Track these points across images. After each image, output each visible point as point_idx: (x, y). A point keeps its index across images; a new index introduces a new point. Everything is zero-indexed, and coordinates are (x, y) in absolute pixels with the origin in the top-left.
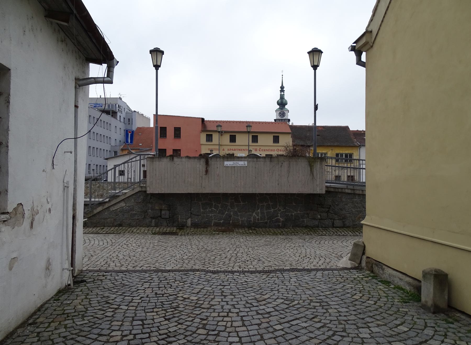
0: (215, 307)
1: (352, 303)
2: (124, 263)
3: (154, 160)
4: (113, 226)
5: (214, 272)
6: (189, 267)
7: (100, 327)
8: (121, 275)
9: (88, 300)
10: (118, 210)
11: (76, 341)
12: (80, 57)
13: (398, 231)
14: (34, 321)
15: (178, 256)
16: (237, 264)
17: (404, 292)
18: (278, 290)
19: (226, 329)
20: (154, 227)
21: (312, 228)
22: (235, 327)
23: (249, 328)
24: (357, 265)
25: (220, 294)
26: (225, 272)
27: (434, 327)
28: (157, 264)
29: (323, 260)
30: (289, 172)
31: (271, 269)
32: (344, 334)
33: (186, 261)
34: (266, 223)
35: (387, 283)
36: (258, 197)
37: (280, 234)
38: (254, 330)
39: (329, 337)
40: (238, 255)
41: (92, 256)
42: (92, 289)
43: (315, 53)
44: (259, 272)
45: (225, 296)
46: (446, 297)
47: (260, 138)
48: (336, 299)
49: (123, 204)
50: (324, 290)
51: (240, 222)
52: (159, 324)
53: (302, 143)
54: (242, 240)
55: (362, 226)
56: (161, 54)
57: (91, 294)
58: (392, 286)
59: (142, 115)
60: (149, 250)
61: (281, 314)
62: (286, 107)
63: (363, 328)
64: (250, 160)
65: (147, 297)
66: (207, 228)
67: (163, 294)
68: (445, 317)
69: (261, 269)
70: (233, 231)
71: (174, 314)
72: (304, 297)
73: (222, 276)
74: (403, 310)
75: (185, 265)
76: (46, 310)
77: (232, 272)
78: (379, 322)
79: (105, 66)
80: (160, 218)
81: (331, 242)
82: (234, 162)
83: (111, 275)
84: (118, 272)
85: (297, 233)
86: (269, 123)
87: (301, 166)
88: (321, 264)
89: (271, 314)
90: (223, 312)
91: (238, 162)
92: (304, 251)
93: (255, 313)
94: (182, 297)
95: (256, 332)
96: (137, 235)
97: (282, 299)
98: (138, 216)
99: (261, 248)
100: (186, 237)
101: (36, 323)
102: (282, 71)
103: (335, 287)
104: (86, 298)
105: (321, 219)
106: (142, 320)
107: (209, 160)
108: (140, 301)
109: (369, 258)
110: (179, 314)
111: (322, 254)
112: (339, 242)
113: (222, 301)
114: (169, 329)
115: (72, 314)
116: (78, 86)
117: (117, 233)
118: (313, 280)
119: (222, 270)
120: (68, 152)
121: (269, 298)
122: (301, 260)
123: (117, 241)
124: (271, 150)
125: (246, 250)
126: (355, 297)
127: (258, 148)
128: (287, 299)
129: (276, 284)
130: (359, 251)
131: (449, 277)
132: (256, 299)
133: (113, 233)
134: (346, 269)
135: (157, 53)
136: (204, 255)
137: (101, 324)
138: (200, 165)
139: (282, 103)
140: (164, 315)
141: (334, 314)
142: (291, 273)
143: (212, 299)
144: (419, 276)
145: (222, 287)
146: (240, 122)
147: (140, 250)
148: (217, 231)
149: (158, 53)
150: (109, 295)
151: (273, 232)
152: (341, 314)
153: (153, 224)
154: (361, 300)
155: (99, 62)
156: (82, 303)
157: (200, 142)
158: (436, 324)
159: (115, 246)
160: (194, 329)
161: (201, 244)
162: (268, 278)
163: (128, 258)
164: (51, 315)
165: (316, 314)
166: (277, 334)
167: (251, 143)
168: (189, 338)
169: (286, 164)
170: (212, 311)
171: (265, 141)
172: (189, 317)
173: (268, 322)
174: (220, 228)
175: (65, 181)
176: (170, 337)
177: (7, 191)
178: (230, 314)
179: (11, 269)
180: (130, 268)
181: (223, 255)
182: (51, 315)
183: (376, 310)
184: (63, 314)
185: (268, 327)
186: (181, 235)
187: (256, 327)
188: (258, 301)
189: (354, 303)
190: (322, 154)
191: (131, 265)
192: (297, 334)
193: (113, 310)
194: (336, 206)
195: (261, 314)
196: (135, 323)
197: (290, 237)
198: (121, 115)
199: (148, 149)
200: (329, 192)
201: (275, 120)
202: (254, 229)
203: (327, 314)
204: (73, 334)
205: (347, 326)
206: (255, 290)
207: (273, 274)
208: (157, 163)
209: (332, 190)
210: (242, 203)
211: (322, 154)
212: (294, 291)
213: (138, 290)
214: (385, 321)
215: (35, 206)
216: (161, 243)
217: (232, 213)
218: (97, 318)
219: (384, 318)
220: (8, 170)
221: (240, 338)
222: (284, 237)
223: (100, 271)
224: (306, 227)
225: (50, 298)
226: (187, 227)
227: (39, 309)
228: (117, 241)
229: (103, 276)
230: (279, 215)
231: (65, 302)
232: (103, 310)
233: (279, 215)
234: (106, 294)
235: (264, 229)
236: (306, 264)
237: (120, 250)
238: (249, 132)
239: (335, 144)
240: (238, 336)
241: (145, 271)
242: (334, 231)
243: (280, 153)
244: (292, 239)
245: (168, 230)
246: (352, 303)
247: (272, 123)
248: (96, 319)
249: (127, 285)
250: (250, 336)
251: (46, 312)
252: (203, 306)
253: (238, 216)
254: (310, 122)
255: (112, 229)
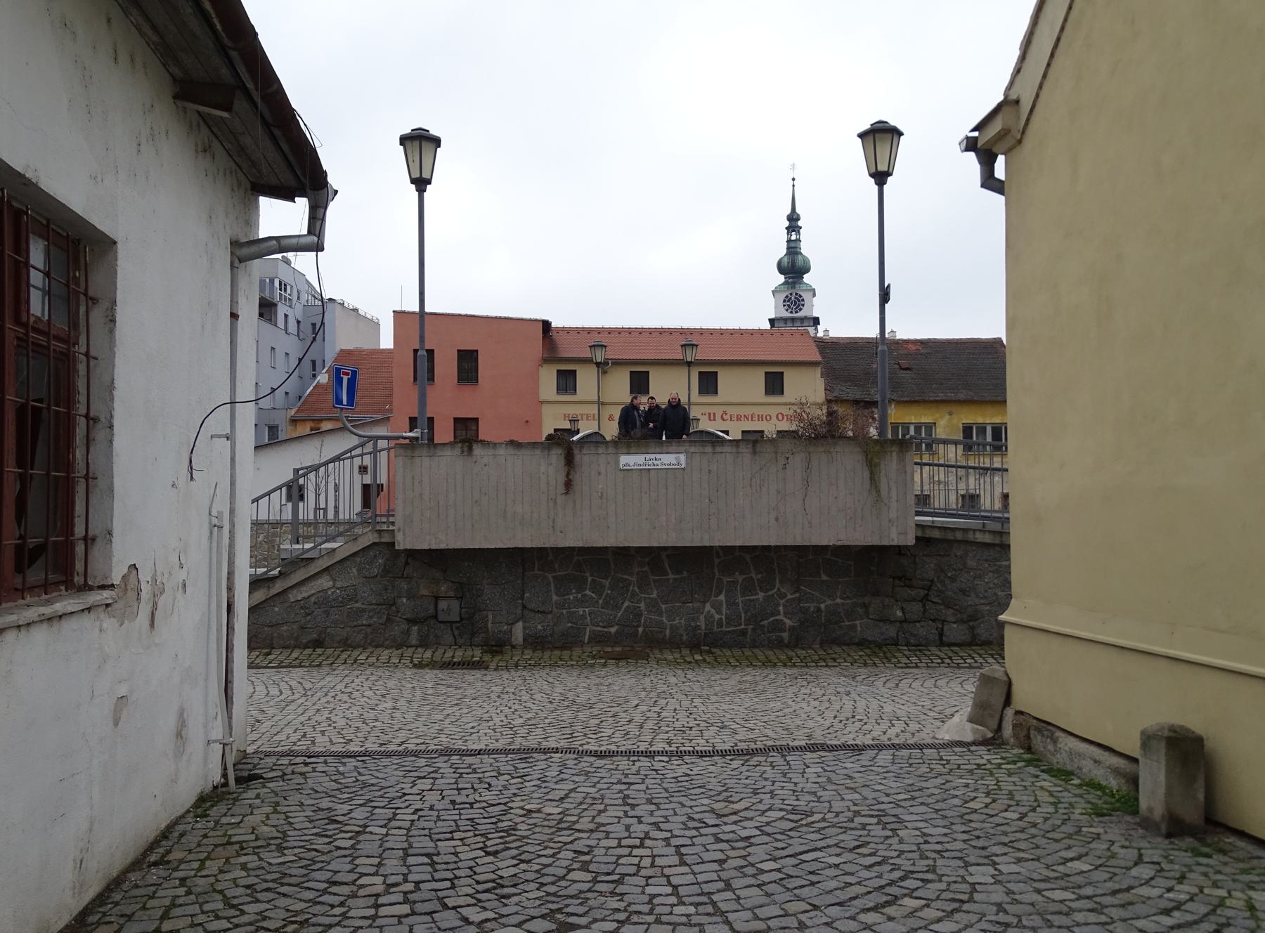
0: (609, 828)
1: (961, 817)
2: (352, 736)
3: (416, 453)
4: (296, 647)
5: (600, 755)
6: (532, 742)
7: (329, 867)
8: (352, 762)
9: (283, 816)
10: (313, 599)
11: (279, 893)
12: (239, 185)
13: (1089, 637)
14: (163, 856)
15: (497, 720)
16: (661, 736)
17: (1104, 793)
18: (772, 792)
19: (638, 871)
20: (417, 647)
21: (880, 646)
22: (662, 867)
23: (697, 868)
24: (990, 735)
25: (620, 801)
26: (628, 754)
27: (1158, 863)
28: (443, 738)
29: (899, 726)
30: (807, 482)
31: (753, 746)
32: (930, 876)
33: (523, 731)
34: (744, 633)
35: (1064, 774)
36: (718, 556)
37: (785, 665)
38: (708, 872)
39: (892, 883)
40: (664, 714)
41: (258, 721)
42: (284, 794)
43: (880, 137)
44: (723, 754)
45: (633, 806)
46: (1201, 796)
47: (726, 379)
48: (923, 809)
49: (324, 583)
50: (893, 791)
51: (668, 632)
52: (472, 863)
53: (856, 394)
54: (673, 680)
55: (1002, 625)
56: (432, 146)
57: (286, 803)
58: (1076, 782)
59: (356, 310)
60: (415, 705)
61: (777, 840)
62: (807, 278)
63: (978, 865)
64: (693, 449)
65: (431, 808)
66: (570, 649)
67: (471, 804)
68: (1196, 844)
69: (727, 747)
70: (647, 657)
71: (506, 842)
72: (837, 806)
73: (624, 763)
74: (1092, 830)
75: (518, 740)
76: (182, 835)
77: (650, 755)
78: (1022, 855)
79: (302, 203)
80: (432, 622)
81: (929, 683)
82: (648, 456)
83: (325, 762)
84: (343, 757)
85: (835, 660)
86: (752, 332)
87: (844, 467)
88: (893, 734)
89: (752, 840)
90: (629, 837)
91: (658, 456)
92: (848, 705)
93: (711, 839)
94: (522, 808)
95: (714, 876)
96: (371, 669)
97: (781, 810)
98: (371, 617)
99: (727, 699)
100: (513, 673)
101: (168, 862)
102: (793, 167)
103: (924, 784)
104: (275, 812)
105: (905, 621)
106: (428, 855)
107: (576, 451)
108: (416, 817)
109: (1022, 713)
110: (518, 844)
111: (900, 713)
112: (952, 684)
113: (627, 816)
114: (499, 873)
115: (252, 844)
116: (237, 261)
117: (310, 666)
118: (865, 770)
119: (623, 749)
120: (219, 436)
121: (746, 809)
122: (837, 726)
123: (318, 686)
124: (760, 418)
125: (686, 703)
126: (971, 805)
127: (719, 411)
128: (794, 811)
129: (766, 779)
130: (997, 701)
131: (1208, 744)
132: (713, 811)
133: (300, 666)
134: (960, 744)
135: (420, 143)
136: (568, 714)
137: (329, 863)
138: (550, 467)
139: (793, 268)
140: (481, 845)
141: (913, 840)
142: (809, 755)
143: (600, 812)
144: (1132, 747)
145: (624, 787)
146: (661, 331)
147: (389, 705)
148: (601, 658)
149: (424, 143)
150: (331, 805)
151: (762, 658)
152: (929, 839)
153: (414, 639)
154: (985, 811)
155: (287, 194)
156: (269, 822)
157: (538, 394)
158: (1166, 857)
159: (315, 699)
160: (562, 872)
161: (559, 689)
162: (745, 768)
163: (360, 724)
164: (199, 845)
165: (868, 839)
166: (765, 878)
167: (695, 397)
168: (552, 889)
169: (797, 461)
170: (602, 835)
171: (740, 388)
172: (545, 848)
173: (744, 857)
174: (609, 649)
175: (214, 513)
176: (503, 886)
177: (110, 534)
178: (648, 843)
179: (116, 724)
180: (372, 746)
181: (623, 715)
182: (199, 845)
183: (1022, 831)
184: (229, 843)
185: (742, 867)
186: (496, 669)
187: (715, 866)
188: (719, 816)
189: (966, 817)
190: (918, 428)
191: (371, 739)
192: (814, 878)
193: (349, 835)
194: (948, 581)
195: (727, 841)
196: (411, 860)
197: (814, 672)
198: (290, 312)
199: (380, 417)
200: (925, 541)
201: (772, 321)
202: (710, 652)
203: (895, 840)
204: (266, 881)
205: (940, 862)
206: (712, 793)
207: (760, 759)
208: (426, 461)
209: (936, 534)
210: (671, 576)
211: (918, 428)
212: (814, 793)
213: (405, 794)
214: (1039, 852)
215: (158, 573)
216: (443, 689)
217: (642, 606)
218: (315, 850)
219: (1037, 847)
220: (112, 484)
221: (675, 887)
222: (795, 671)
223: (290, 753)
224: (862, 644)
225: (183, 811)
226: (513, 647)
227: (165, 834)
228: (318, 686)
229: (306, 764)
230: (781, 608)
231: (224, 820)
232: (326, 836)
233: (781, 608)
234: (325, 803)
235: (737, 652)
236: (851, 736)
237: (332, 706)
238: (689, 364)
239: (962, 396)
240: (669, 883)
241: (416, 754)
242: (942, 655)
243: (785, 426)
244: (817, 678)
245: (459, 655)
246: (961, 817)
247: (761, 332)
248: (314, 853)
249: (373, 785)
250: (698, 883)
251: (183, 840)
252: (577, 826)
253: (660, 614)
254: (872, 332)
255: (295, 655)
